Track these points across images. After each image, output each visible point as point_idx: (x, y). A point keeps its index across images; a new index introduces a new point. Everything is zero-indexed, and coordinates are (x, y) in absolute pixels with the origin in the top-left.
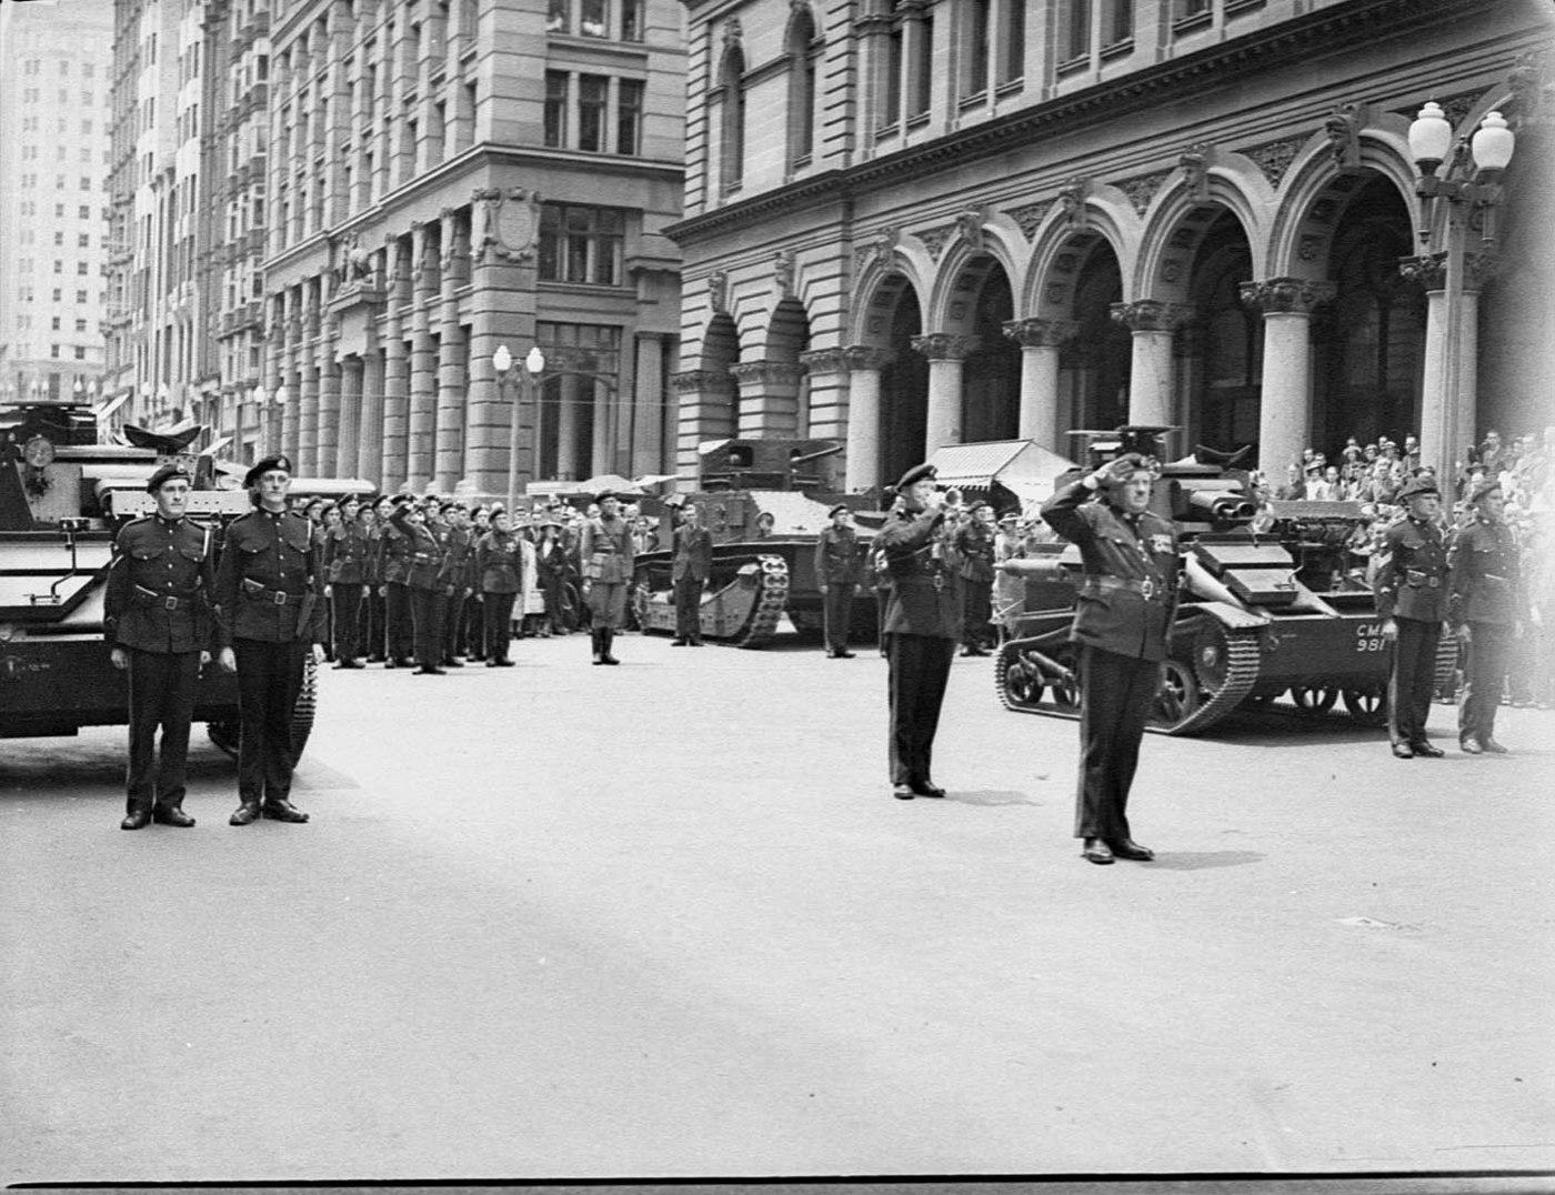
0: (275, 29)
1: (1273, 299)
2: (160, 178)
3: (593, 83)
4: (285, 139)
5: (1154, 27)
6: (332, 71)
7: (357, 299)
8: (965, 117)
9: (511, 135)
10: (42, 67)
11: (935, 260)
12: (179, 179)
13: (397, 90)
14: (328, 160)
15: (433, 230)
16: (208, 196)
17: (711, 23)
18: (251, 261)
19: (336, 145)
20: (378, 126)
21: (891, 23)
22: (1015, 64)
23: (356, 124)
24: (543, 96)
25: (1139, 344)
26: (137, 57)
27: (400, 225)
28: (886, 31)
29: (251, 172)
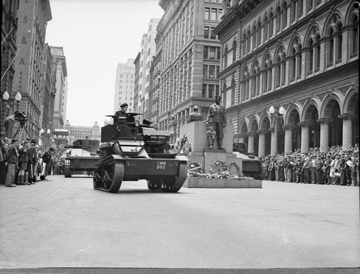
0: (161, 74)
1: (344, 117)
2: (142, 100)
3: (211, 86)
4: (162, 94)
5: (346, 56)
6: (169, 82)
7: (172, 124)
8: (277, 88)
9: (196, 96)
10: (123, 76)
11: (302, 106)
12: (145, 100)
13: (179, 86)
14: (187, 85)
15: (184, 112)
16: (150, 104)
17: (222, 79)
18: (156, 116)
19: (170, 95)
20: (176, 93)
21: (294, 57)
22: (340, 56)
23: (173, 92)
24: (202, 89)
25: (322, 127)
26: (139, 76)
27: (179, 111)
28: (352, 28)
29: (157, 99)
